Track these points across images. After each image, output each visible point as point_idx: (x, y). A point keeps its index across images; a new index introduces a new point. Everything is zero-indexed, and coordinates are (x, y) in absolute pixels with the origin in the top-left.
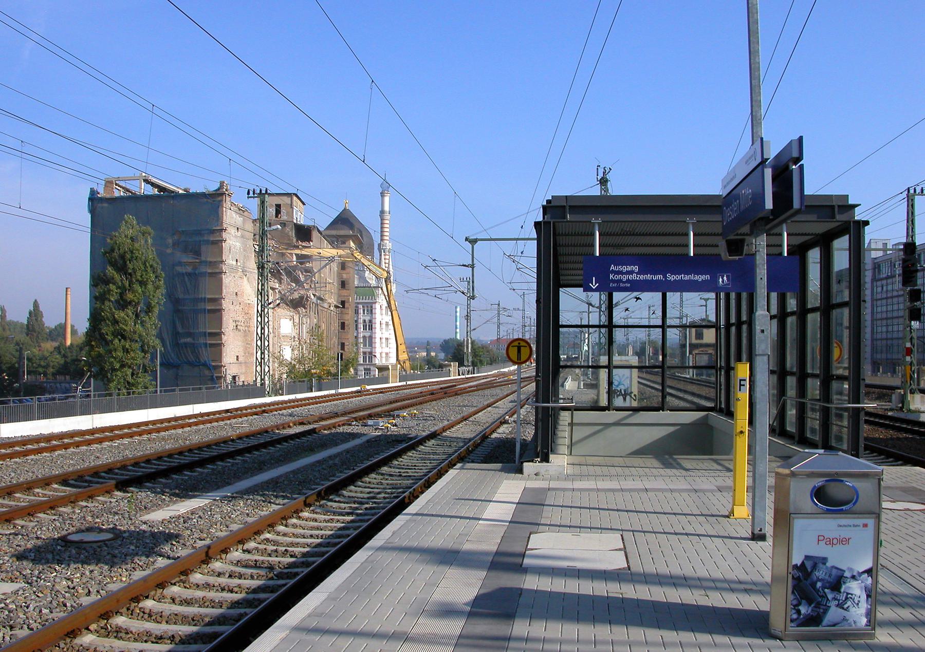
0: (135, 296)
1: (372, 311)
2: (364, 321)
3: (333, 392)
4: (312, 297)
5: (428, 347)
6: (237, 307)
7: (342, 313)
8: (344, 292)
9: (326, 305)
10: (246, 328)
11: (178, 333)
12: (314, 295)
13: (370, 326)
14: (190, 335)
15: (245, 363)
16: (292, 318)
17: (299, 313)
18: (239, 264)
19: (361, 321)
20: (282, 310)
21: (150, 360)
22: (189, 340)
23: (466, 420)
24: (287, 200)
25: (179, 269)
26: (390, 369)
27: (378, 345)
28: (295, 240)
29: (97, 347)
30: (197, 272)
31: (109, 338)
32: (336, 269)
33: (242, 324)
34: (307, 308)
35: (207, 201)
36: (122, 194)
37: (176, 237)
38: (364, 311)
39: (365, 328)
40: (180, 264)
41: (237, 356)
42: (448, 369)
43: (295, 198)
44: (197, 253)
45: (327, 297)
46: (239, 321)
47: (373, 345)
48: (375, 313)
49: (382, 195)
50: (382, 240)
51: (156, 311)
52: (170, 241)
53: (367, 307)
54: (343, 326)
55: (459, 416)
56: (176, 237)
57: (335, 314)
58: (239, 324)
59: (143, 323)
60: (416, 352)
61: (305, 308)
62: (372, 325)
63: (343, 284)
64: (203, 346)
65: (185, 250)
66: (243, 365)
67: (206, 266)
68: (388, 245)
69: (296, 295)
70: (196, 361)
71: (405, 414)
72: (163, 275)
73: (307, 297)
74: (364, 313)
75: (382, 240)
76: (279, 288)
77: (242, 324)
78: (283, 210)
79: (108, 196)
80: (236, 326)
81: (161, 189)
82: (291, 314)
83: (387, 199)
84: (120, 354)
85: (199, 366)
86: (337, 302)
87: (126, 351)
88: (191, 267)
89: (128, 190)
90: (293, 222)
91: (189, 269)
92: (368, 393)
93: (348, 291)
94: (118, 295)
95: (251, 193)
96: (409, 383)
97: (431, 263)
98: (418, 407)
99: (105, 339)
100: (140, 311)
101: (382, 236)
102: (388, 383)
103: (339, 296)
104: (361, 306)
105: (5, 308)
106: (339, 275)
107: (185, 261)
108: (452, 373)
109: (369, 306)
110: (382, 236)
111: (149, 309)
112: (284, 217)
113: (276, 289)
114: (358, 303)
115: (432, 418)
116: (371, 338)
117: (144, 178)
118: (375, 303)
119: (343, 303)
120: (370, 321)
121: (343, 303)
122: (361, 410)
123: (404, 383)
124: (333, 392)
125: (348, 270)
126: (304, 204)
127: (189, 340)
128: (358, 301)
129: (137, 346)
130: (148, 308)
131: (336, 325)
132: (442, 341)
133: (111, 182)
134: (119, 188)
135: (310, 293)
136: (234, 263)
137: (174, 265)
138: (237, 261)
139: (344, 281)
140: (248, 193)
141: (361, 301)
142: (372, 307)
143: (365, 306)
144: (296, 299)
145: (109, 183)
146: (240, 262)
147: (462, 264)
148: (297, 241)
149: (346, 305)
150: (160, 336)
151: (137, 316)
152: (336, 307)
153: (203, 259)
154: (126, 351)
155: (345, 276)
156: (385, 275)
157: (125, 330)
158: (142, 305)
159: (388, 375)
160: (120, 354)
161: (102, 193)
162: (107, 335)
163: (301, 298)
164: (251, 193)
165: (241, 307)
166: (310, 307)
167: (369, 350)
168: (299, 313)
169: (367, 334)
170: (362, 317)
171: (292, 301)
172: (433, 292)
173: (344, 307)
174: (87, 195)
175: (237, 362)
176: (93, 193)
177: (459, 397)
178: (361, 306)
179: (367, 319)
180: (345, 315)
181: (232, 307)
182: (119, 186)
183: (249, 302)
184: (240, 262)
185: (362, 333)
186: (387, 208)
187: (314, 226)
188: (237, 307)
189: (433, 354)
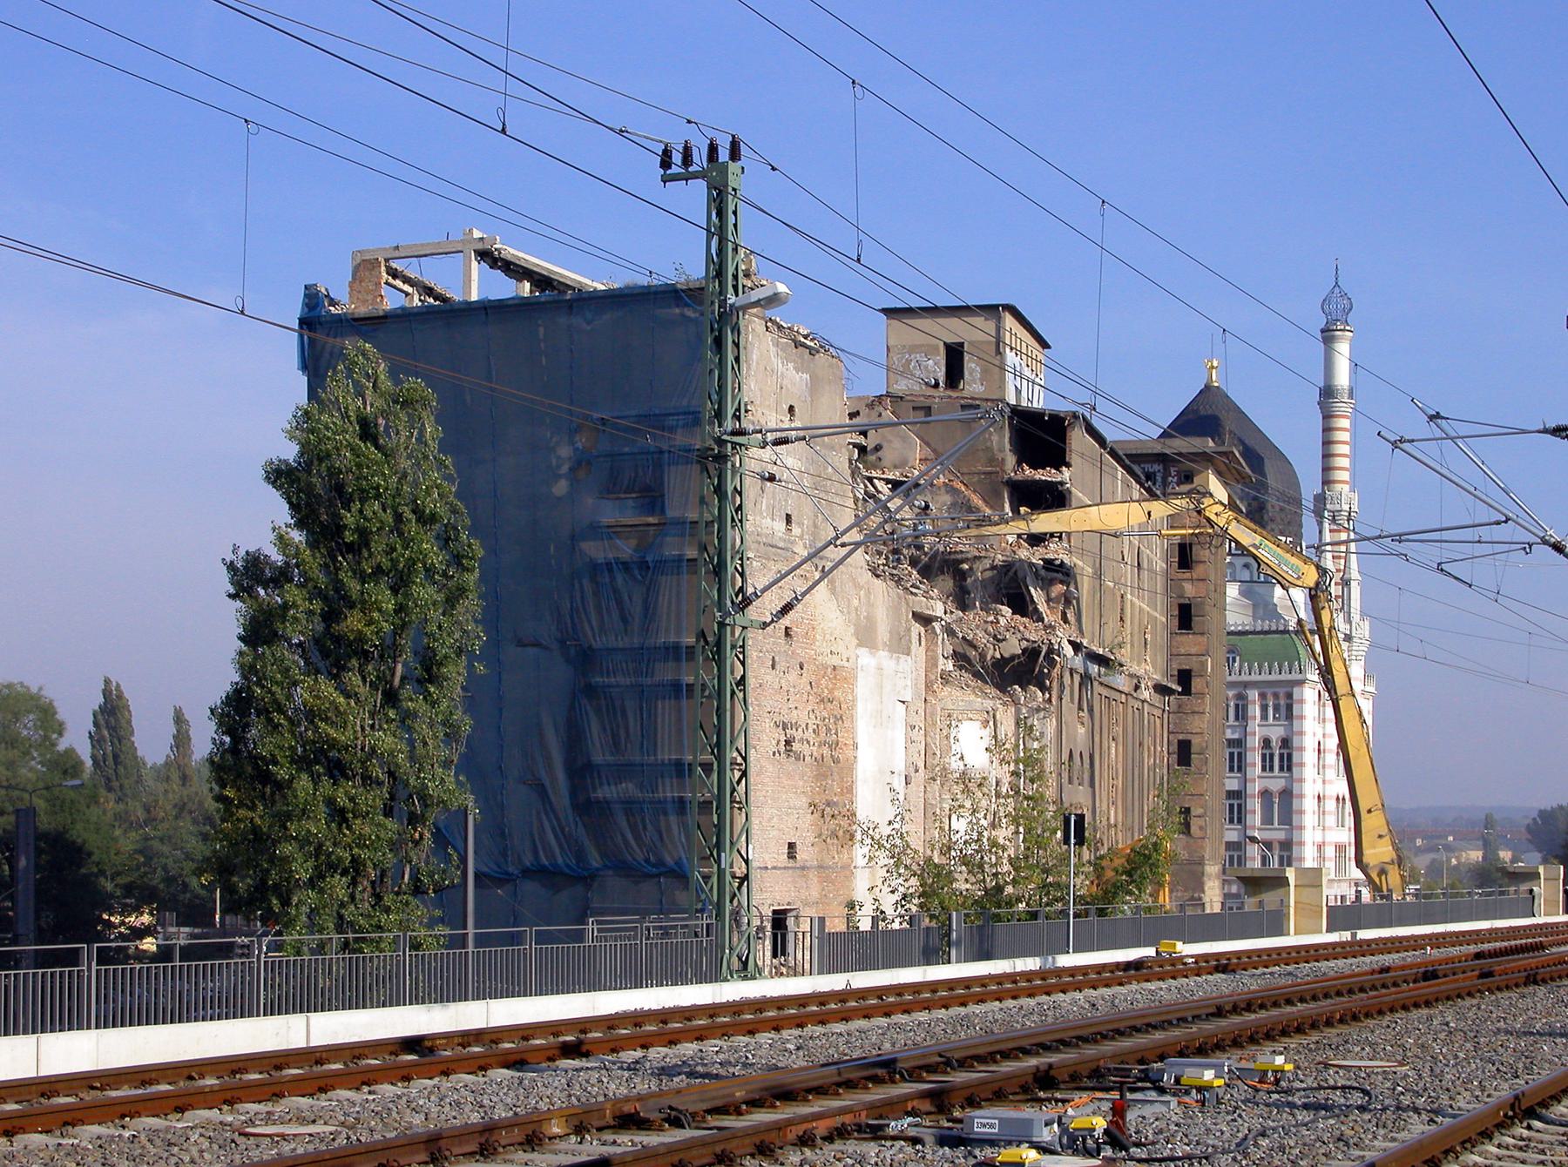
0: (370, 623)
1: (1289, 708)
2: (1266, 743)
3: (1031, 964)
4: (1068, 650)
5: (1487, 830)
6: (793, 676)
7: (1180, 710)
8: (1189, 643)
9: (1121, 682)
10: (826, 751)
11: (589, 767)
12: (1077, 647)
13: (1284, 757)
14: (624, 771)
15: (821, 867)
16: (990, 719)
17: (1016, 703)
18: (796, 530)
19: (1254, 742)
20: (957, 693)
21: (434, 852)
22: (629, 788)
23: (1531, 1113)
24: (985, 324)
25: (595, 550)
26: (1292, 882)
27: (1309, 819)
28: (1011, 460)
29: (241, 805)
30: (649, 559)
31: (282, 773)
32: (1160, 565)
33: (809, 735)
34: (1049, 689)
35: (683, 315)
36: (416, 302)
37: (581, 441)
38: (1264, 708)
39: (1267, 765)
40: (595, 531)
41: (791, 846)
42: (1524, 887)
43: (1009, 321)
44: (652, 498)
45: (1124, 655)
46: (796, 726)
47: (1295, 817)
48: (1301, 717)
49: (1328, 335)
50: (1327, 482)
51: (455, 674)
52: (565, 451)
53: (1276, 696)
54: (1184, 752)
55: (1503, 1091)
56: (581, 441)
57: (1158, 713)
58: (798, 735)
59: (406, 718)
60: (1448, 848)
61: (1043, 688)
62: (1290, 756)
63: (1185, 617)
64: (669, 807)
65: (612, 488)
66: (813, 875)
67: (683, 535)
68: (1345, 495)
69: (1013, 647)
70: (647, 861)
71: (1209, 1075)
72: (480, 553)
73: (1051, 651)
74: (1264, 717)
75: (1327, 482)
76: (948, 618)
77: (809, 735)
78: (971, 366)
79: (363, 311)
80: (788, 743)
81: (542, 282)
82: (988, 704)
83: (1343, 348)
84: (317, 826)
85: (658, 876)
86: (1166, 674)
87: (339, 816)
88: (633, 542)
89: (429, 291)
90: (1003, 400)
91: (626, 549)
92: (1172, 968)
93: (1200, 638)
94: (317, 619)
95: (677, 158)
96: (1365, 934)
97: (1422, 429)
98: (1293, 1042)
99: (266, 778)
100: (403, 678)
101: (1327, 469)
102: (1279, 930)
103: (1172, 655)
104: (1253, 695)
105: (184, 711)
106: (1172, 584)
107: (612, 521)
108: (1540, 903)
109: (1282, 691)
110: (1327, 469)
111: (429, 671)
112: (974, 383)
113: (936, 619)
114: (1246, 685)
115: (1357, 1098)
116: (1287, 795)
117: (480, 246)
118: (1301, 683)
119: (1185, 677)
120: (1286, 743)
121: (1185, 677)
122: (1006, 1055)
123: (1346, 936)
124: (1031, 964)
125: (1198, 571)
126: (1044, 345)
127: (629, 788)
128: (1245, 678)
129: (373, 799)
130: (428, 670)
131: (1158, 753)
132: (1535, 814)
133: (374, 264)
134: (407, 288)
135: (1062, 638)
136: (780, 526)
137: (575, 538)
138: (788, 519)
139: (1189, 606)
140: (666, 163)
141: (1255, 677)
142: (1290, 696)
143: (1269, 691)
144: (1013, 657)
145: (364, 268)
146: (800, 524)
147: (1552, 425)
148: (1019, 463)
149: (1196, 684)
150: (471, 767)
151: (391, 698)
152: (1161, 689)
153: (672, 513)
154: (339, 816)
155: (1189, 590)
156: (1311, 577)
157: (333, 744)
158: (407, 655)
159: (1284, 903)
160: (317, 826)
161: (346, 302)
162: (275, 763)
163: (1032, 653)
164: (677, 158)
165: (805, 680)
166: (1062, 685)
167: (1281, 835)
168: (1016, 703)
169: (1276, 784)
170: (1259, 729)
171: (1001, 663)
172: (1432, 553)
173: (1187, 691)
174: (293, 312)
175: (791, 863)
176: (313, 298)
177: (1541, 990)
178: (1253, 695)
179: (1276, 733)
180: (1190, 718)
181: (770, 677)
182: (407, 280)
183: (835, 661)
184: (800, 524)
185: (1257, 780)
186: (1342, 378)
187: (1075, 416)
188: (793, 676)
189: (1505, 855)
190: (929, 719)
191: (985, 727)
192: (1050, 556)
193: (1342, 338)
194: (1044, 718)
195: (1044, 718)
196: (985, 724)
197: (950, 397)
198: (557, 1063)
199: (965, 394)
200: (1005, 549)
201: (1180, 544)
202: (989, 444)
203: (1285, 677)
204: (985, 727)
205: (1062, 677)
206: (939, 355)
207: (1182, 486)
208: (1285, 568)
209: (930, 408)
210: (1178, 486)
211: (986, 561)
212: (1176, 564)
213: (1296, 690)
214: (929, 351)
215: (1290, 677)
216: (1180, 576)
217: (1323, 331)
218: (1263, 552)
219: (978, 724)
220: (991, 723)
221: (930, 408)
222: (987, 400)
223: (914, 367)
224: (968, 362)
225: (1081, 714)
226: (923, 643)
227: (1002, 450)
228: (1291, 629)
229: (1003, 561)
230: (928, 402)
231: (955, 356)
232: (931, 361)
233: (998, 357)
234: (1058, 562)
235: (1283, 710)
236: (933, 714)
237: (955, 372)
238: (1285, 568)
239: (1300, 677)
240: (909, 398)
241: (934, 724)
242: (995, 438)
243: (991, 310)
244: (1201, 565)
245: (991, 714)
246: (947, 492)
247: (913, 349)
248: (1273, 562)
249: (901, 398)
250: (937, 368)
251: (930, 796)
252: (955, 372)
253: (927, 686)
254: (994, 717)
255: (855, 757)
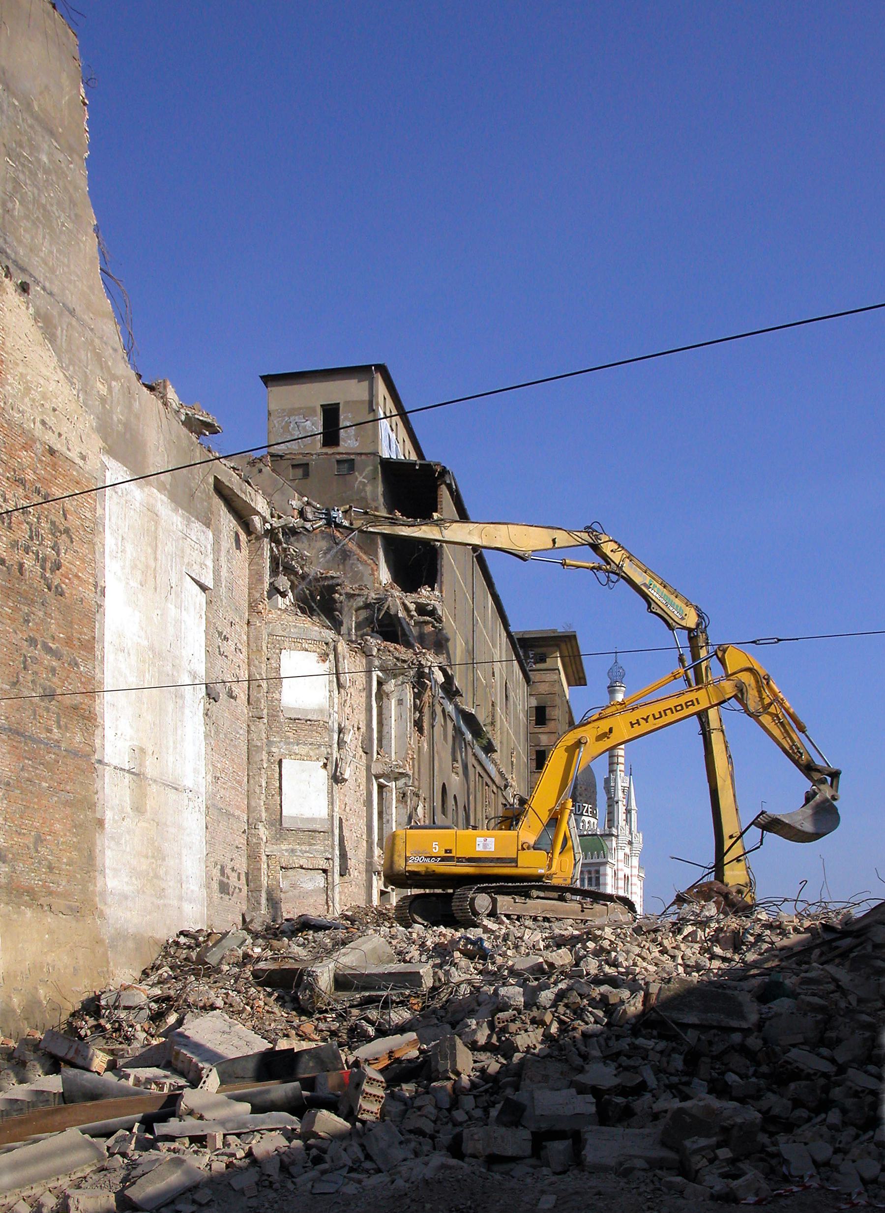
1: (598, 879)
50: (612, 771)
53: (589, 872)
90: (375, 454)
106: (531, 737)
112: (349, 442)
118: (605, 863)
142: (598, 872)
155: (544, 739)
190: (253, 646)
191: (324, 661)
192: (422, 601)
193: (620, 690)
194: (403, 683)
195: (403, 683)
196: (324, 657)
197: (326, 454)
198: (615, 1081)
199: (340, 449)
200: (378, 589)
201: (536, 707)
202: (363, 494)
203: (595, 860)
204: (324, 661)
205: (433, 706)
206: (316, 416)
207: (537, 665)
208: (671, 608)
209: (307, 464)
210: (535, 664)
211: (359, 599)
212: (534, 722)
213: (602, 868)
214: (307, 413)
215: (598, 861)
216: (536, 730)
217: (609, 687)
218: (653, 592)
219: (314, 657)
220: (332, 657)
221: (307, 464)
222: (361, 454)
223: (293, 429)
224: (343, 421)
225: (456, 765)
226: (243, 544)
227: (375, 500)
228: (598, 833)
229: (376, 599)
230: (305, 460)
231: (331, 413)
232: (308, 422)
233: (372, 414)
234: (430, 608)
235: (594, 880)
236: (258, 638)
237: (331, 436)
238: (671, 608)
239: (604, 860)
240: (288, 456)
241: (259, 650)
242: (369, 489)
243: (361, 371)
244: (553, 722)
245: (332, 645)
246: (323, 538)
247: (292, 412)
248: (661, 602)
249: (281, 456)
250: (316, 424)
251: (254, 736)
252: (331, 436)
253: (250, 606)
254: (335, 649)
255: (100, 606)
